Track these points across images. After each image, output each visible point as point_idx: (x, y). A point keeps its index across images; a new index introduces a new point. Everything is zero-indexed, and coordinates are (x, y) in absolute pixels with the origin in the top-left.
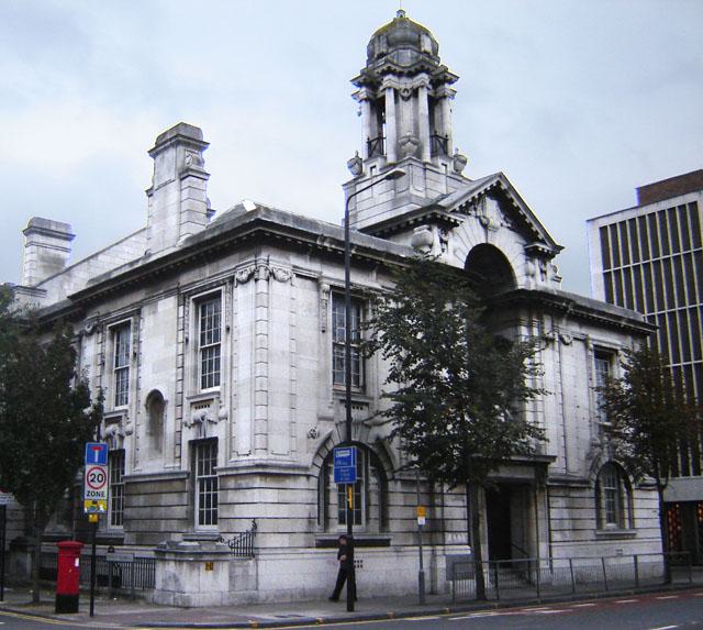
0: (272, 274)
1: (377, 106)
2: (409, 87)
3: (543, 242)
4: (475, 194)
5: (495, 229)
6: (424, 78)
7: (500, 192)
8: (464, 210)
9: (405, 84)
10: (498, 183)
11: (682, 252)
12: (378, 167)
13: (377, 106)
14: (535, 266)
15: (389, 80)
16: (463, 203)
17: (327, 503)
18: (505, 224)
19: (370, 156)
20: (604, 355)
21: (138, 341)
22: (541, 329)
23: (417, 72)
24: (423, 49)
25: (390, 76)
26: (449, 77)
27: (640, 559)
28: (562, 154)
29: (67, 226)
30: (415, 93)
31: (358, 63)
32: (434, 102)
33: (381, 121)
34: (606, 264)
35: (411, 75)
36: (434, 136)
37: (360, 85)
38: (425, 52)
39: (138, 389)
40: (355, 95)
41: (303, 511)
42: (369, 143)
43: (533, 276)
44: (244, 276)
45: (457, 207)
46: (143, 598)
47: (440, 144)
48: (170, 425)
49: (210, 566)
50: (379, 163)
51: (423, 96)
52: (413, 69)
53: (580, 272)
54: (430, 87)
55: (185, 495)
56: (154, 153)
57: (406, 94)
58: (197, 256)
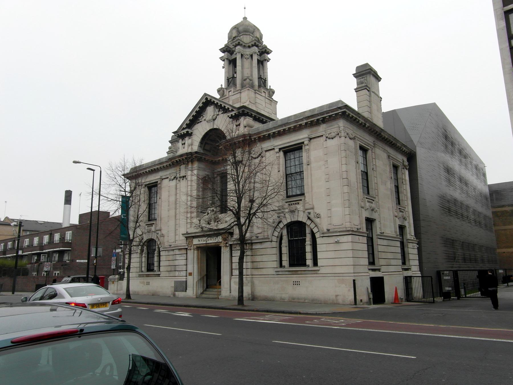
1: (232, 63)
12: (232, 91)
19: (228, 86)
20: (45, 256)
24: (255, 36)
26: (268, 50)
27: (460, 274)
31: (224, 41)
36: (260, 78)
38: (256, 37)
40: (222, 59)
42: (228, 80)
44: (173, 177)
46: (244, 153)
47: (263, 81)
51: (255, 58)
52: (250, 45)
55: (290, 186)
58: (160, 167)
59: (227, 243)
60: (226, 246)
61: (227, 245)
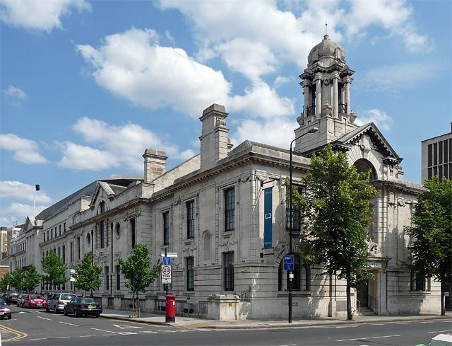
0: (258, 178)
1: (312, 89)
2: (328, 78)
3: (392, 156)
4: (358, 135)
5: (368, 151)
6: (337, 74)
7: (372, 134)
8: (352, 143)
9: (328, 76)
10: (371, 128)
11: (443, 163)
13: (312, 89)
14: (387, 169)
15: (320, 76)
16: (352, 139)
17: (307, 280)
18: (373, 148)
21: (198, 208)
22: (388, 199)
23: (333, 70)
25: (319, 73)
28: (398, 115)
29: (163, 153)
30: (331, 82)
32: (341, 86)
33: (314, 97)
34: (430, 164)
35: (330, 72)
37: (304, 78)
39: (199, 230)
41: (199, 277)
43: (386, 173)
44: (245, 179)
45: (348, 141)
48: (213, 246)
49: (230, 305)
50: (312, 119)
52: (330, 69)
53: (413, 173)
54: (339, 78)
56: (202, 119)
57: (326, 83)
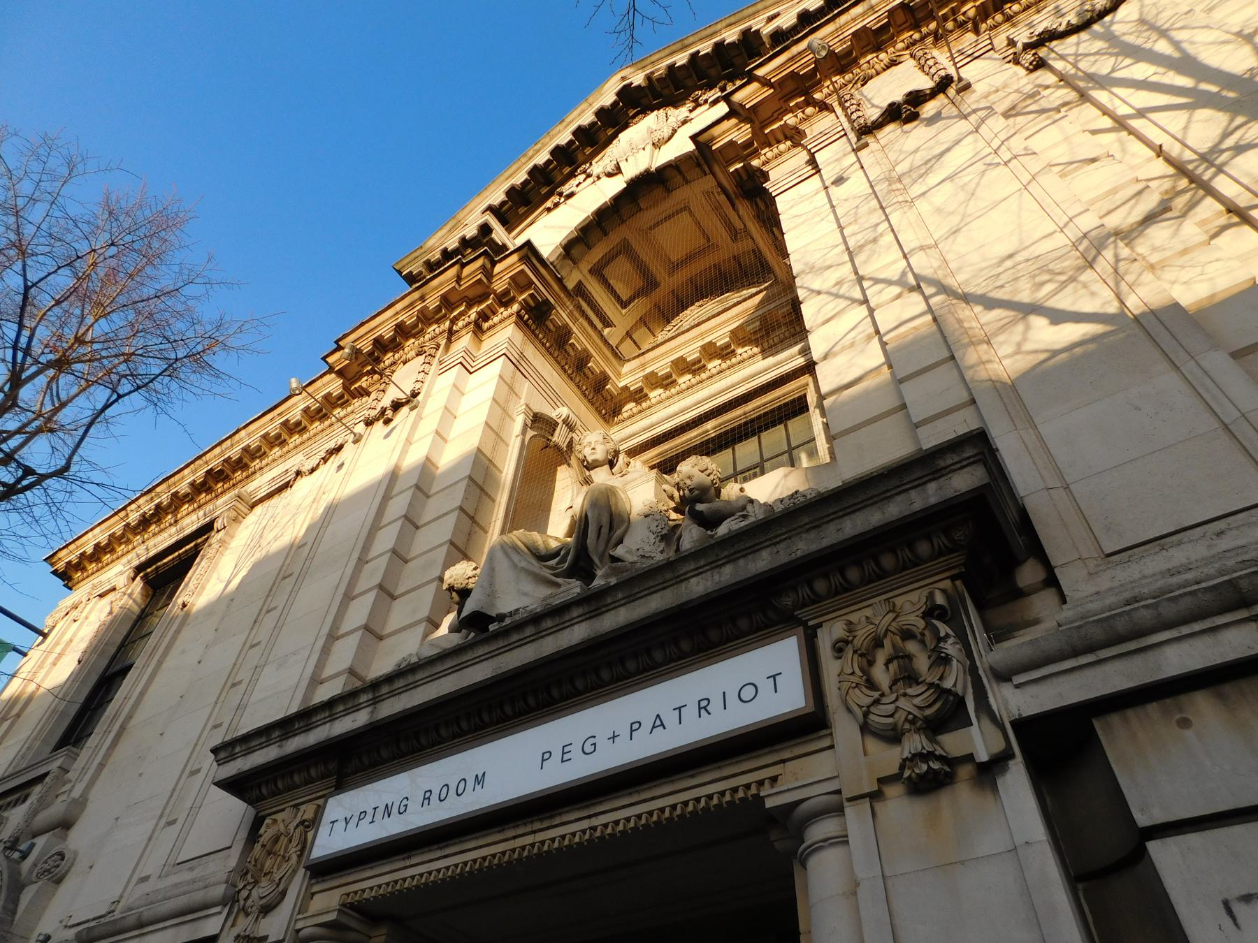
59: (949, 714)
60: (928, 781)
61: (978, 740)
